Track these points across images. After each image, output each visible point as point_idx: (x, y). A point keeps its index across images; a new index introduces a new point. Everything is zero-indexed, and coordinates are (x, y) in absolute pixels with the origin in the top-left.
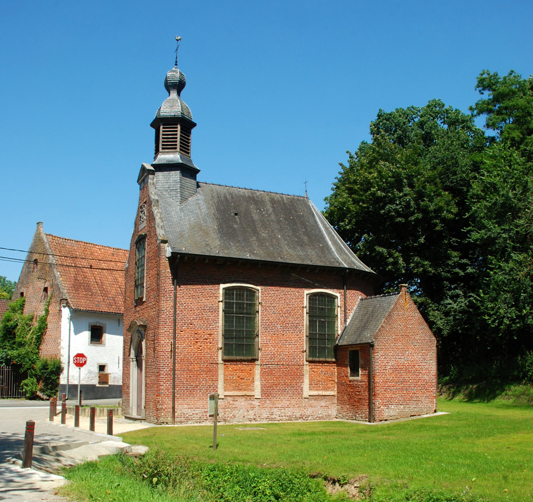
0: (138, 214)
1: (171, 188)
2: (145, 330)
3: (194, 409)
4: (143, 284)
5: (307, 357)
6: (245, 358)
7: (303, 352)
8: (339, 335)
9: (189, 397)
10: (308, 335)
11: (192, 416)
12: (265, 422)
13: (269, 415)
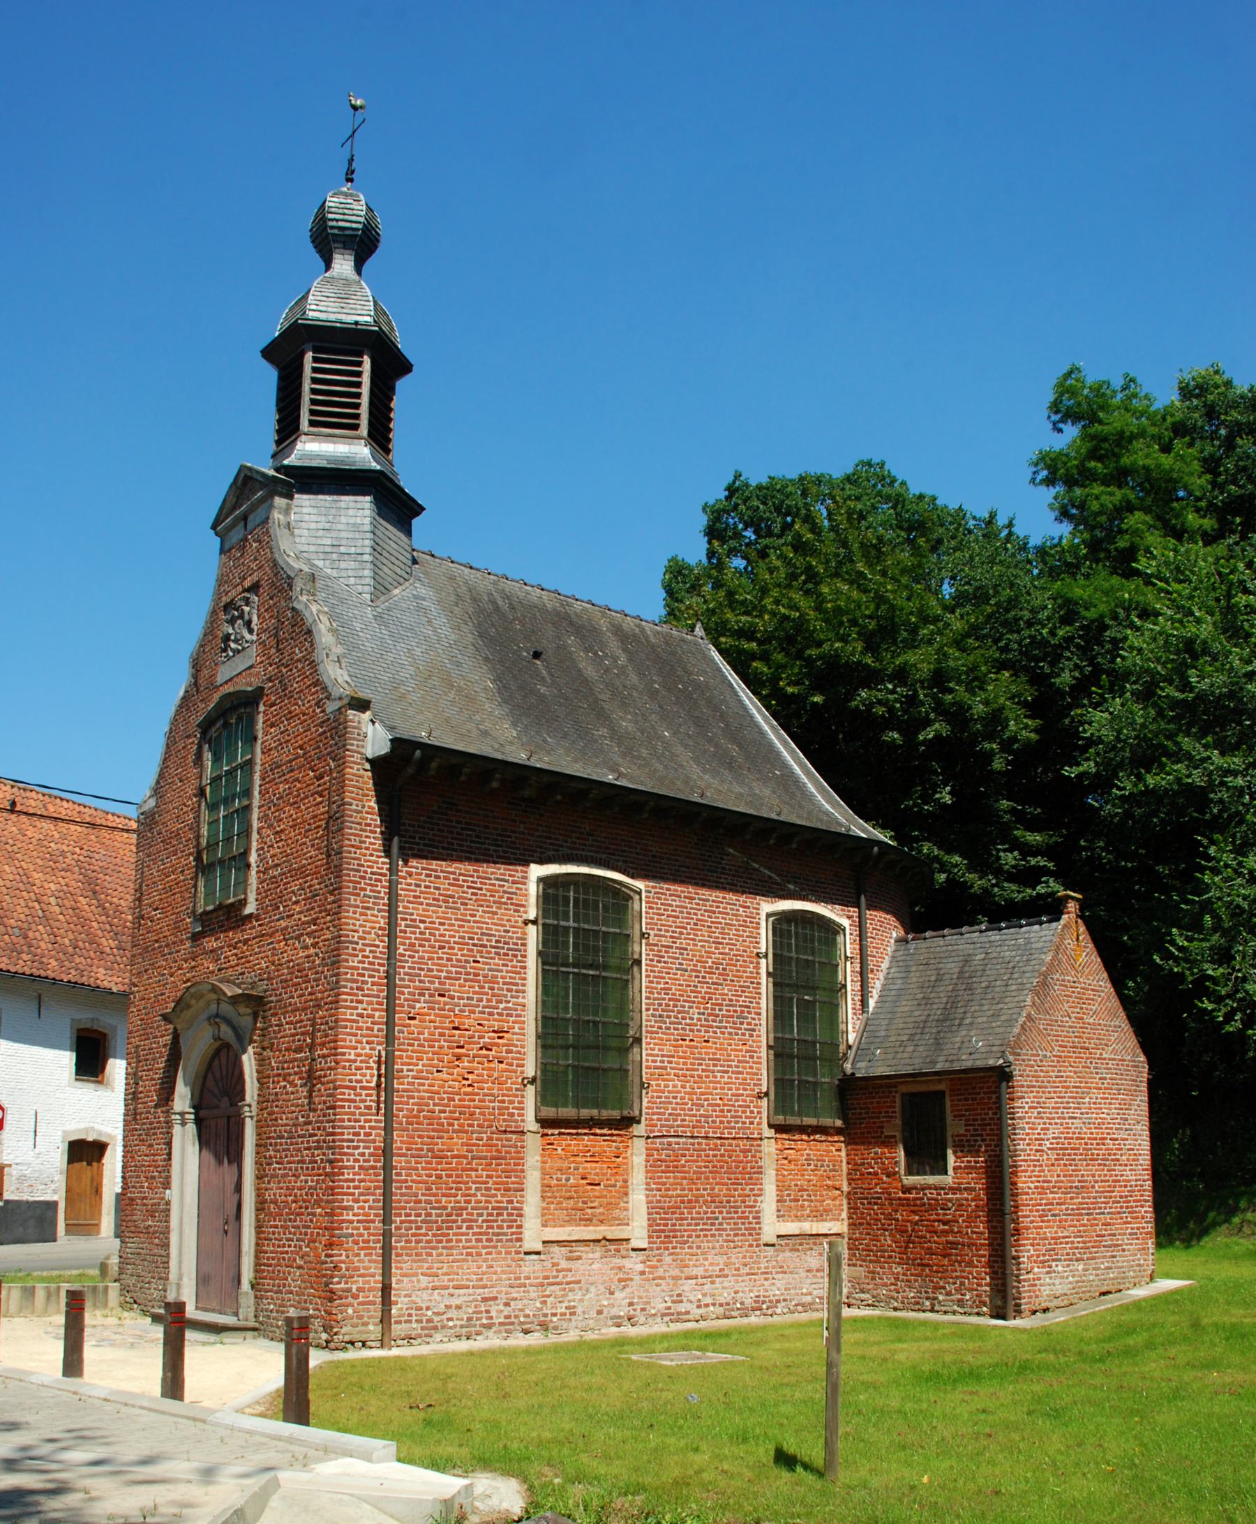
0: (210, 631)
1: (343, 549)
2: (255, 1016)
3: (451, 1291)
4: (246, 854)
5: (772, 1112)
6: (605, 1114)
7: (760, 1098)
8: (850, 1047)
9: (437, 1248)
10: (771, 1043)
11: (445, 1317)
12: (659, 1327)
13: (669, 1304)
